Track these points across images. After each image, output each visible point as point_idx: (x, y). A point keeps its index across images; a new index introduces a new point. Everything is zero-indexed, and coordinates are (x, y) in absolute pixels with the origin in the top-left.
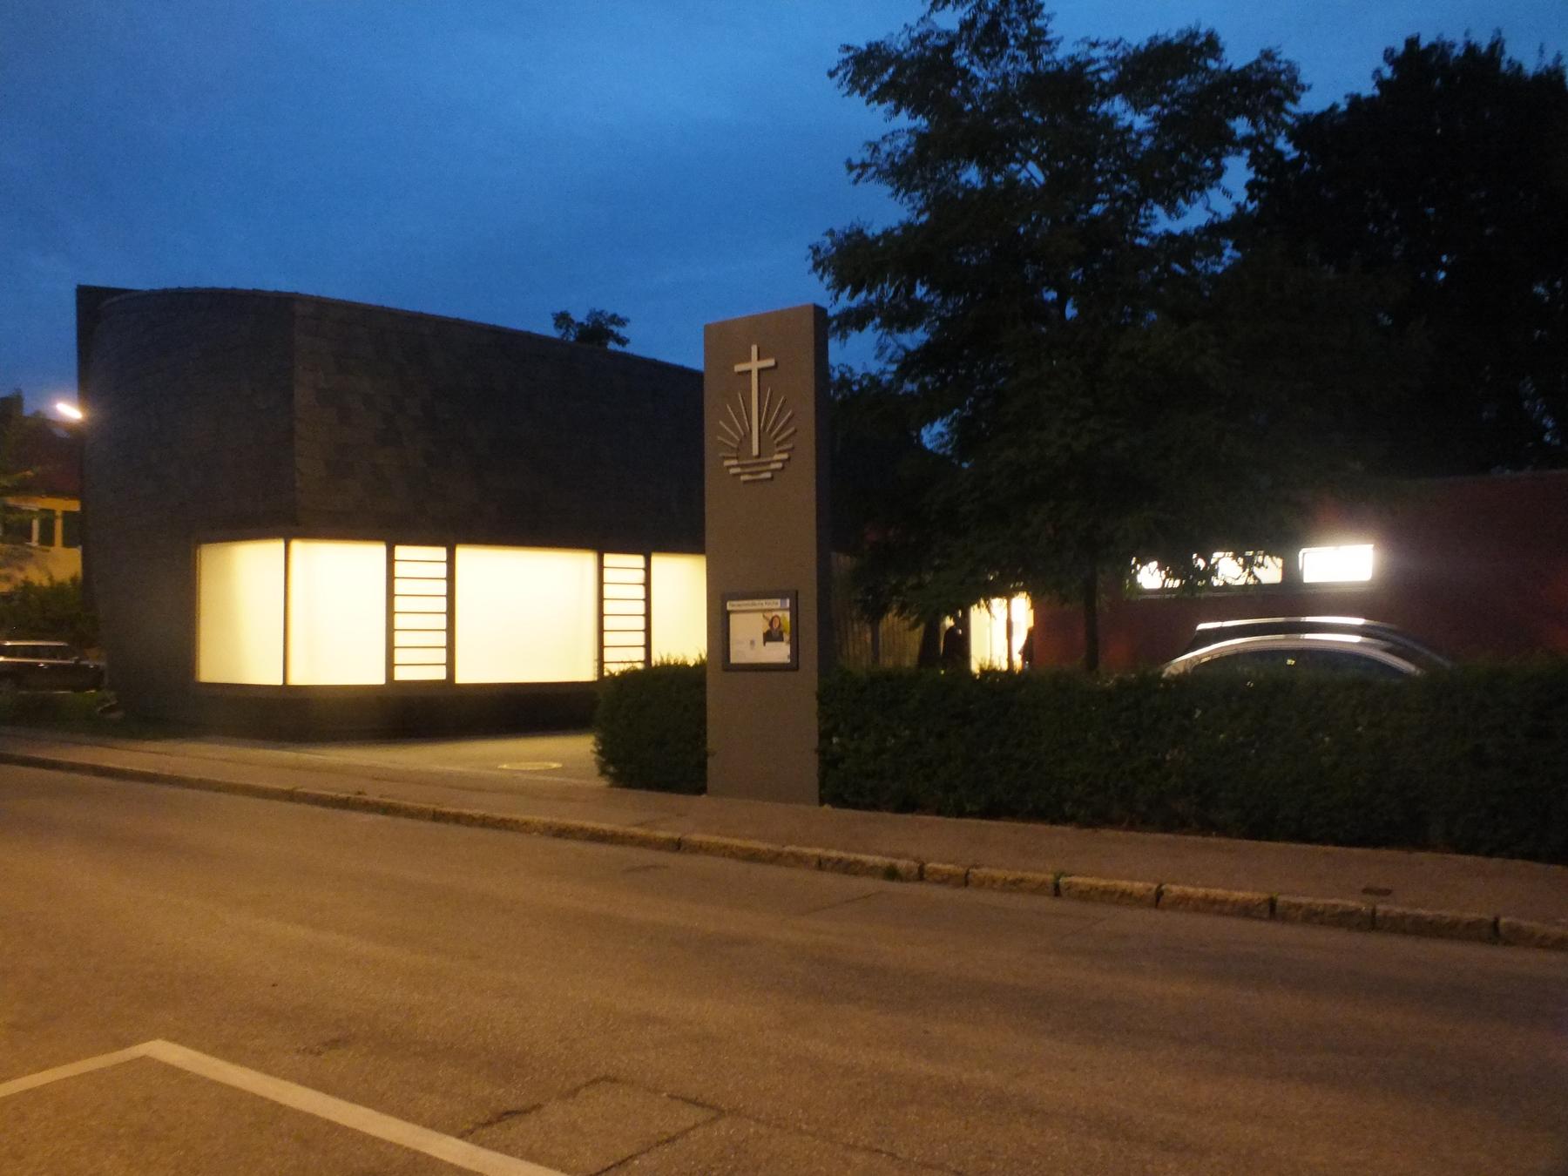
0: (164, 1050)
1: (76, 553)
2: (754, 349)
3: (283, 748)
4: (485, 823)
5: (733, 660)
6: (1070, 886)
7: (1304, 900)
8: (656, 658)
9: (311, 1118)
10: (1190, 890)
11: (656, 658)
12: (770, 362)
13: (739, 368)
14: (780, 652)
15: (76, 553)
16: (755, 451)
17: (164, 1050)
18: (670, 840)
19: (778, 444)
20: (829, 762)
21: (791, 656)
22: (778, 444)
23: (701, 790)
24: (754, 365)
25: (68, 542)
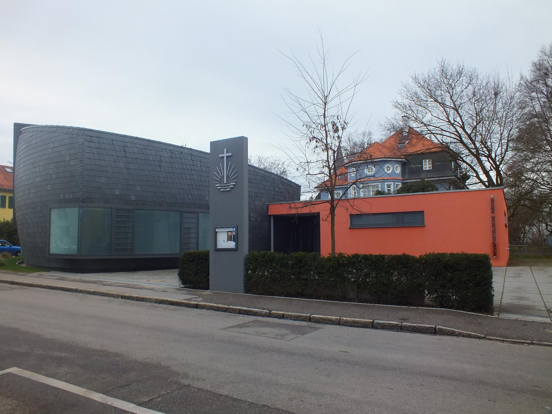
0: (13, 370)
1: (12, 210)
2: (225, 150)
3: (71, 274)
4: (138, 299)
5: (219, 247)
6: (314, 318)
7: (381, 322)
8: (337, 251)
9: (29, 380)
10: (348, 319)
11: (337, 251)
12: (230, 154)
13: (220, 156)
14: (232, 245)
15: (12, 210)
16: (225, 182)
17: (13, 370)
18: (306, 317)
19: (232, 180)
20: (247, 278)
21: (235, 246)
22: (232, 180)
23: (207, 287)
24: (225, 155)
25: (10, 207)
